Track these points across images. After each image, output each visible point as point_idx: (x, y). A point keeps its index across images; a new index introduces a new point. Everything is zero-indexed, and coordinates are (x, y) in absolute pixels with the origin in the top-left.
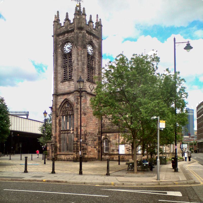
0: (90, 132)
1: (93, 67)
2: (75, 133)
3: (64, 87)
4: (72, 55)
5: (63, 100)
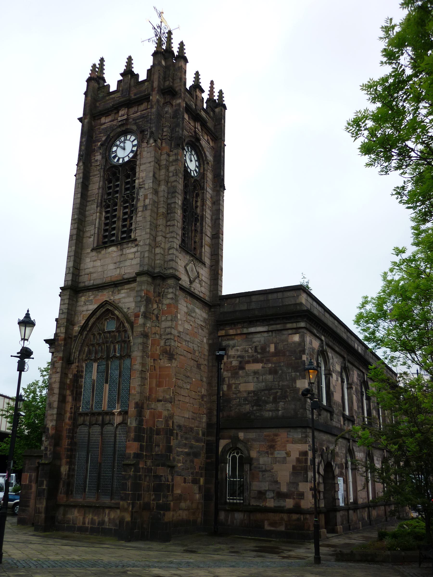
0: (182, 422)
2: (132, 423)
5: (93, 307)
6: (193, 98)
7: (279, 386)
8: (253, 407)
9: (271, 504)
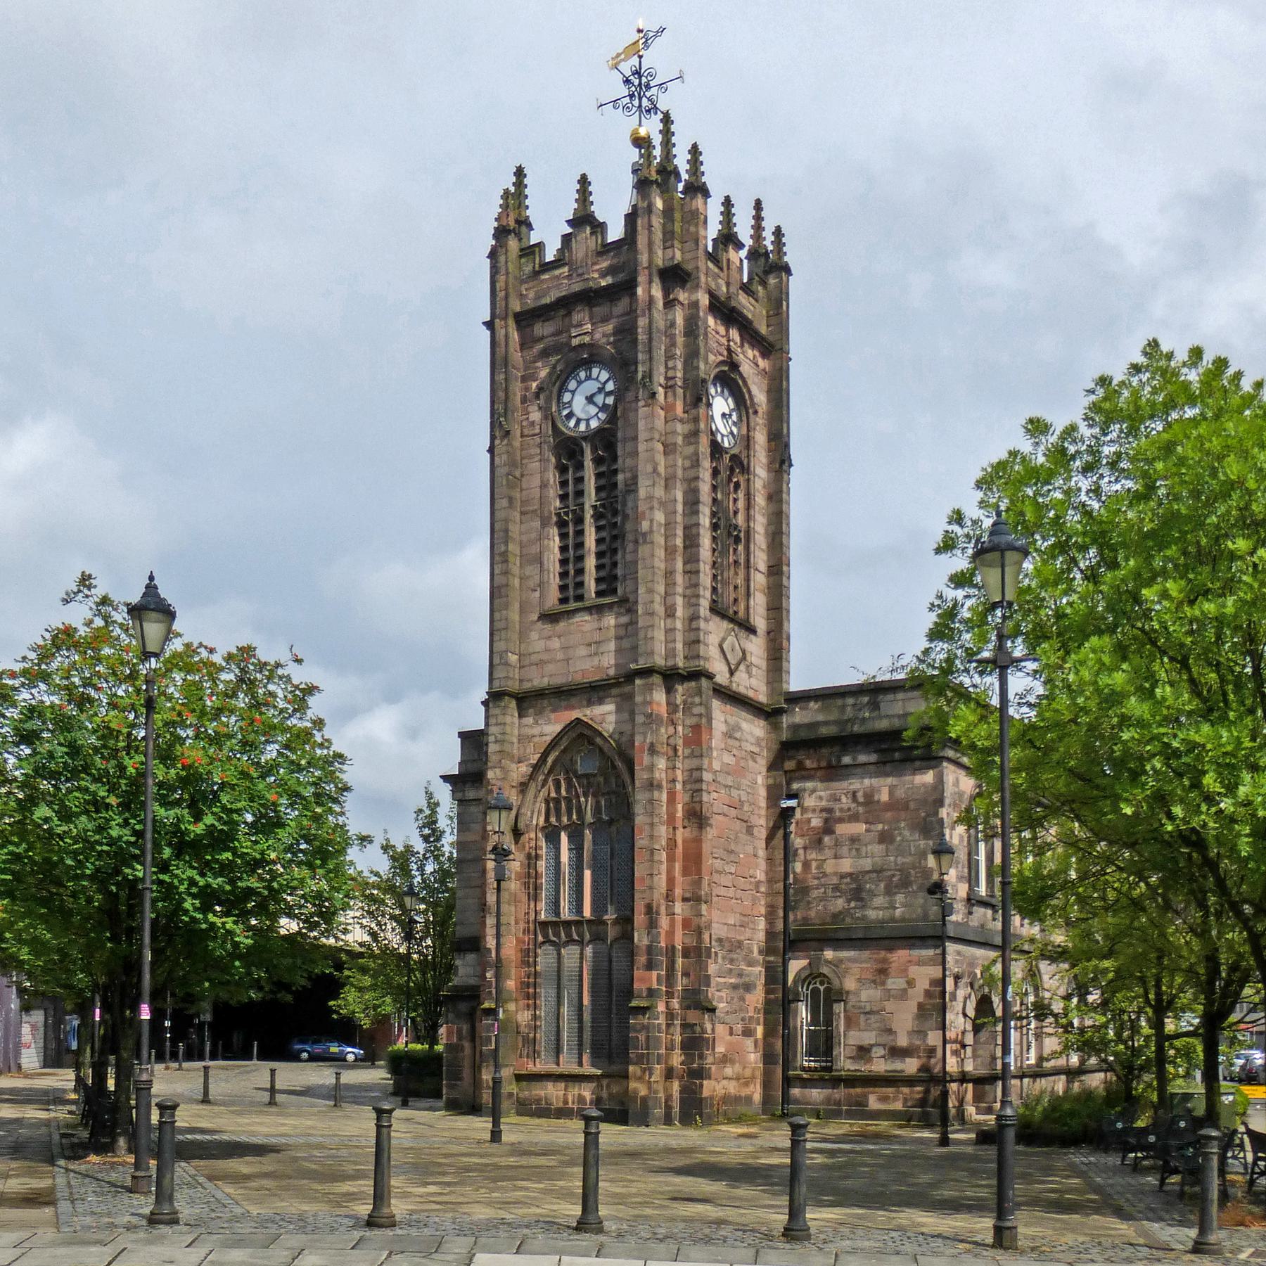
0: (723, 934)
1: (736, 527)
3: (565, 648)
4: (620, 446)
6: (721, 269)
7: (896, 864)
8: (849, 901)
9: (880, 1066)
